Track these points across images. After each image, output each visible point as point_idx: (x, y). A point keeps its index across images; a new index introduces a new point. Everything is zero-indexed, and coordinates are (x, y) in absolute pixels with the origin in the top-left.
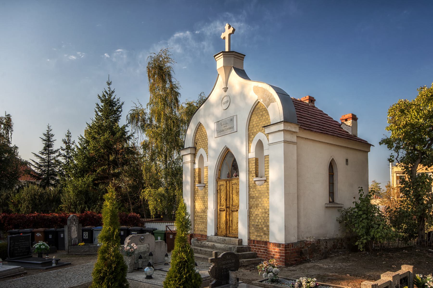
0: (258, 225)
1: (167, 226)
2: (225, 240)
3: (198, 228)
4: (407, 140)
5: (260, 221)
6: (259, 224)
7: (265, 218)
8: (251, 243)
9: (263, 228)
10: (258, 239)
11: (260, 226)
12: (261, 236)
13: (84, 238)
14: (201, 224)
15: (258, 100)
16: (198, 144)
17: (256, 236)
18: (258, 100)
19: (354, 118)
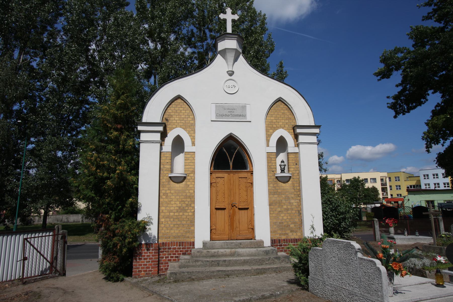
0: (282, 223)
1: (26, 239)
2: (241, 244)
3: (320, 237)
4: (111, 247)
5: (285, 218)
6: (283, 221)
7: (291, 215)
8: (275, 243)
9: (289, 226)
10: (283, 237)
11: (285, 224)
12: (287, 234)
13: (450, 188)
14: (178, 228)
15: (235, 109)
16: (170, 121)
17: (280, 234)
18: (235, 109)
19: (388, 104)
